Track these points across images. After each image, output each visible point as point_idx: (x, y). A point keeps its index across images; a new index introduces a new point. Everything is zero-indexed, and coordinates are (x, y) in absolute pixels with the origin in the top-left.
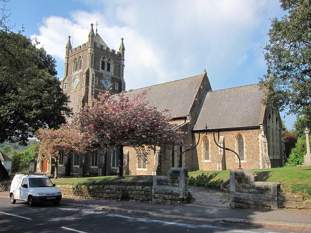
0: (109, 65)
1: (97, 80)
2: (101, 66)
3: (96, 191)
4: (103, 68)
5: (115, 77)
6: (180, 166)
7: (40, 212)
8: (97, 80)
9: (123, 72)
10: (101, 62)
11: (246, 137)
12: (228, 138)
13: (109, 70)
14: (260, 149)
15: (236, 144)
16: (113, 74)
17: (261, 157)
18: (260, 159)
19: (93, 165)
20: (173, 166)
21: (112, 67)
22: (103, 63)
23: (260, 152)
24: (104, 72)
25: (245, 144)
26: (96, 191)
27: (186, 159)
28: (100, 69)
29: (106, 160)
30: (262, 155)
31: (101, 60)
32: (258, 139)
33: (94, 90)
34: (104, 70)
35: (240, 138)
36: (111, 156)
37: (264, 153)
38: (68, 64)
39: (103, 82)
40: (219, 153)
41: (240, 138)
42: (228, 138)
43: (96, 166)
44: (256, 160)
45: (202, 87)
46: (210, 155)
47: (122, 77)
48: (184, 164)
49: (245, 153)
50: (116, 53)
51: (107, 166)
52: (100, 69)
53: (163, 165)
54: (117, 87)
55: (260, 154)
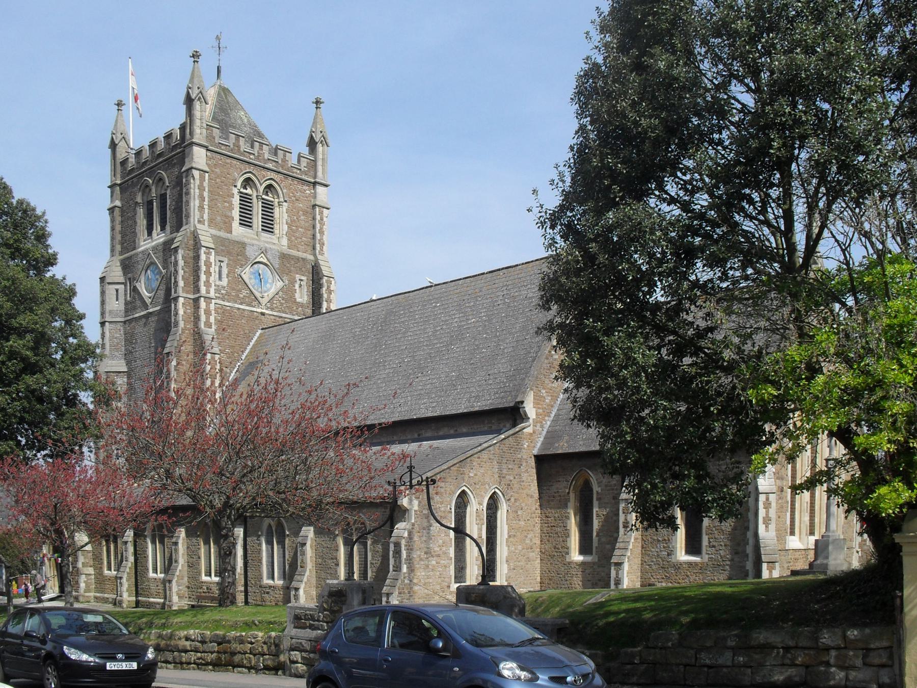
0: (268, 208)
1: (225, 271)
2: (236, 213)
4: (246, 221)
5: (294, 252)
7: (385, 558)
8: (225, 271)
10: (236, 200)
13: (268, 226)
16: (285, 241)
21: (281, 214)
22: (245, 200)
27: (510, 552)
28: (236, 224)
31: (235, 191)
33: (212, 306)
38: (431, 286)
39: (247, 274)
45: (737, 440)
50: (293, 160)
52: (236, 224)
53: (420, 573)
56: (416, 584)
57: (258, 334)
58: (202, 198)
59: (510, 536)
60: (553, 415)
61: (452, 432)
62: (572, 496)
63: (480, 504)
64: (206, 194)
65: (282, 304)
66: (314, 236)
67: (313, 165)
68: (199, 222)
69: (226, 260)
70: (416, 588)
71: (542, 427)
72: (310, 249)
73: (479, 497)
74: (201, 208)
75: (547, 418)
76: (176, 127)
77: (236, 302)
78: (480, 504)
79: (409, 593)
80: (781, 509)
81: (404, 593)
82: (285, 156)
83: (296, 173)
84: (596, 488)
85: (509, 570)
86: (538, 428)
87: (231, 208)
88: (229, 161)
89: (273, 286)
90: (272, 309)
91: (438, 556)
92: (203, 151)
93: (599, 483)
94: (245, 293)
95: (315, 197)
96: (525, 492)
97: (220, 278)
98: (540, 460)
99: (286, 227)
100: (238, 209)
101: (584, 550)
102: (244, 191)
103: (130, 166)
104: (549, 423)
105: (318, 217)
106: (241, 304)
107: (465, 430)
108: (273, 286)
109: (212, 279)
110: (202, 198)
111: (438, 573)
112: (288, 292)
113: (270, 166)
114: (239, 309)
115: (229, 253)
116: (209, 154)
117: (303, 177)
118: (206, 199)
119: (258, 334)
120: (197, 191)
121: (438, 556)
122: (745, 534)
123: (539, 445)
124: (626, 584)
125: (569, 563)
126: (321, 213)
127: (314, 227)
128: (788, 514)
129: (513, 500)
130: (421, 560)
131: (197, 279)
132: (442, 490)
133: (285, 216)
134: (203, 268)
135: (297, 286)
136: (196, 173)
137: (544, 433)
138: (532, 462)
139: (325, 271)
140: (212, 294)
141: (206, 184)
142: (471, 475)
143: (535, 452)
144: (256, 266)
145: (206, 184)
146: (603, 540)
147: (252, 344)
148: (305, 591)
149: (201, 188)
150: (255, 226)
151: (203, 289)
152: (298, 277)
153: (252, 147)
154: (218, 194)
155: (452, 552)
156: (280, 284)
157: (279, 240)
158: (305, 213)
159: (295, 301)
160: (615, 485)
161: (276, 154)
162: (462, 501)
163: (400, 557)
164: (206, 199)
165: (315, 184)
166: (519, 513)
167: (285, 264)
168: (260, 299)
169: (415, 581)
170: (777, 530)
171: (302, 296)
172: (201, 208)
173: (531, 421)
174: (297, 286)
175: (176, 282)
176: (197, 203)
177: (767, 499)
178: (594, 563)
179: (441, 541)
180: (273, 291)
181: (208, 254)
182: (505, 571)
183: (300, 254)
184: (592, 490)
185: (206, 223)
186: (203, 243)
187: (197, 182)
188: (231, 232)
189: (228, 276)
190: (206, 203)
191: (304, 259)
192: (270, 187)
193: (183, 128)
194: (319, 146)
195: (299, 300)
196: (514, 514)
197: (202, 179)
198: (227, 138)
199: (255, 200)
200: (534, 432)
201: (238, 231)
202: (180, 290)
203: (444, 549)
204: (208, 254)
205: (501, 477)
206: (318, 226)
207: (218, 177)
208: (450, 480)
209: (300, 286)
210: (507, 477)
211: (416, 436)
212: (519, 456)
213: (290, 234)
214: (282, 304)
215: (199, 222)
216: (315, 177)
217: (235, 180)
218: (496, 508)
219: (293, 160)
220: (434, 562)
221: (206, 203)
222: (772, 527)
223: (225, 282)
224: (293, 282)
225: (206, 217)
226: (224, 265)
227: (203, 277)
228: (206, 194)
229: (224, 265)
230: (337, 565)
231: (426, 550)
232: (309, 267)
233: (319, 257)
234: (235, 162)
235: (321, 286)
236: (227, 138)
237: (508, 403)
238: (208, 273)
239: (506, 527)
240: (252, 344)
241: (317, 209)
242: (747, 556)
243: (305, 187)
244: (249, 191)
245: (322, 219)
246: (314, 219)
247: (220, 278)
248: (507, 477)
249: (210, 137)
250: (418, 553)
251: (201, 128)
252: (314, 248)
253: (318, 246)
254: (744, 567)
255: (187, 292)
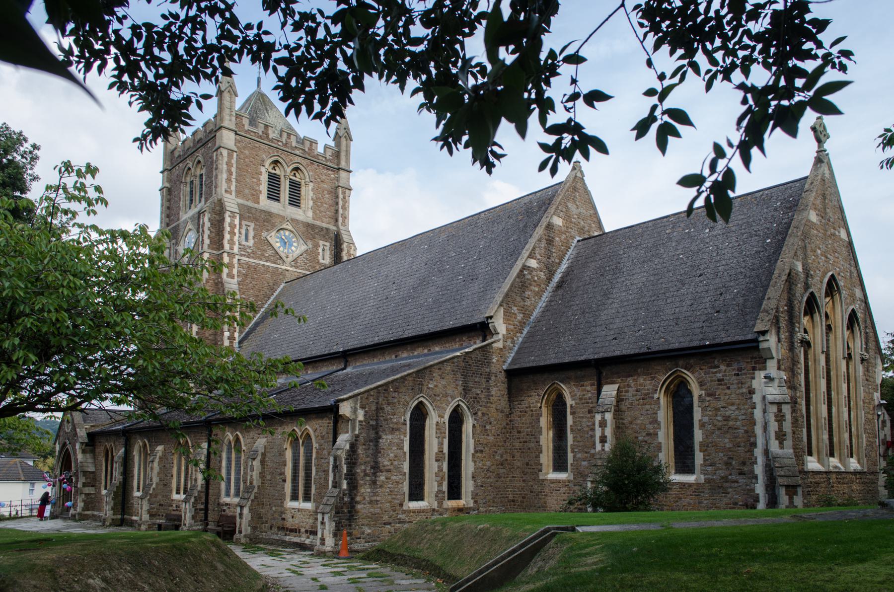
0: (295, 187)
1: (251, 234)
2: (264, 188)
3: (225, 572)
4: (274, 196)
5: (318, 223)
6: (454, 491)
8: (251, 234)
9: (345, 208)
10: (264, 178)
11: (701, 384)
12: (632, 390)
13: (295, 200)
14: (758, 430)
15: (664, 415)
16: (310, 214)
17: (760, 460)
18: (759, 469)
19: (295, 497)
20: (417, 493)
21: (307, 193)
22: (274, 180)
23: (760, 441)
24: (281, 208)
25: (697, 415)
26: (225, 572)
29: (207, 481)
30: (766, 452)
31: (263, 170)
32: (752, 392)
34: (278, 200)
35: (679, 395)
36: (220, 462)
37: (774, 446)
39: (274, 238)
40: (599, 447)
41: (679, 395)
42: (632, 390)
43: (307, 498)
44: (742, 473)
46: (570, 456)
47: (345, 223)
48: (467, 485)
49: (697, 447)
50: (320, 149)
51: (212, 499)
53: (365, 490)
54: (327, 253)
55: (758, 452)
56: (358, 503)
57: (282, 286)
58: (230, 173)
59: (476, 452)
60: (525, 332)
61: (426, 351)
62: (544, 410)
63: (441, 416)
64: (234, 170)
65: (306, 264)
66: (337, 211)
67: (337, 155)
68: (226, 191)
69: (252, 225)
70: (359, 507)
71: (513, 342)
72: (332, 221)
73: (440, 409)
74: (229, 180)
75: (518, 335)
76: (212, 117)
77: (261, 260)
78: (441, 416)
79: (349, 512)
80: (795, 422)
81: (343, 512)
82: (311, 145)
83: (323, 160)
84: (569, 401)
85: (476, 486)
86: (509, 343)
87: (259, 183)
88: (258, 145)
89: (297, 248)
90: (296, 267)
91: (389, 471)
92: (232, 135)
93: (573, 396)
94: (270, 252)
95: (338, 180)
96: (494, 406)
97: (247, 239)
98: (511, 374)
99: (311, 203)
100: (266, 185)
101: (560, 465)
102: (273, 171)
103: (176, 154)
104: (521, 339)
105: (341, 196)
106: (267, 261)
107: (437, 349)
108: (297, 248)
109: (236, 238)
110: (230, 173)
111: (388, 490)
112: (312, 255)
113: (297, 152)
114: (264, 266)
115: (255, 220)
116: (238, 137)
117: (328, 164)
118: (234, 174)
119: (282, 286)
120: (225, 166)
121: (389, 471)
122: (751, 452)
123: (509, 360)
124: (561, 224)
125: (543, 480)
126: (344, 193)
127: (337, 204)
128: (805, 430)
129: (480, 414)
130: (366, 475)
131: (222, 237)
132: (395, 400)
133: (311, 194)
134: (228, 229)
135: (320, 250)
136: (225, 152)
137: (516, 349)
138: (502, 377)
139: (345, 237)
140: (236, 249)
141: (234, 161)
142: (431, 386)
143: (505, 367)
144: (282, 232)
145: (234, 161)
146: (579, 456)
147: (275, 294)
148: (250, 510)
149: (229, 164)
150: (282, 200)
151: (227, 247)
152: (321, 243)
153: (281, 136)
154: (245, 173)
155: (406, 467)
156: (304, 248)
157: (305, 213)
158: (330, 192)
159: (318, 262)
160: (590, 398)
161: (303, 144)
162: (419, 415)
163: (340, 471)
164: (234, 174)
165: (339, 169)
166: (488, 427)
167: (310, 231)
168: (285, 259)
169: (358, 499)
170: (795, 448)
171: (326, 258)
172: (229, 180)
173: (500, 336)
174: (320, 250)
175: (203, 240)
176: (225, 176)
177: (780, 410)
178: (569, 481)
179: (392, 455)
180: (298, 252)
181: (233, 217)
182: (472, 488)
183: (324, 225)
184: (565, 404)
185: (233, 193)
186: (228, 208)
187: (226, 159)
188: (258, 203)
189: (254, 238)
190: (234, 176)
191: (327, 229)
192: (297, 169)
193: (215, 117)
194: (343, 140)
195: (321, 261)
196: (481, 429)
197: (230, 156)
198: (256, 127)
199: (282, 179)
200: (504, 347)
201: (265, 203)
202: (206, 247)
203: (396, 463)
204: (233, 217)
205: (466, 390)
206: (341, 203)
207: (247, 157)
208: (404, 389)
209: (323, 250)
210: (474, 390)
211: (394, 357)
212: (487, 370)
213: (316, 208)
214: (306, 264)
215: (226, 191)
216: (338, 165)
217: (263, 161)
218: (461, 422)
219: (320, 149)
220: (383, 478)
221: (234, 176)
222: (789, 443)
223: (251, 242)
224: (316, 246)
225: (233, 188)
226: (251, 229)
227: (227, 236)
228: (234, 170)
229: (251, 229)
230: (285, 481)
231: (372, 464)
232: (332, 235)
233: (341, 228)
234: (263, 146)
235: (341, 250)
236: (256, 127)
237: (478, 318)
238: (232, 233)
239: (472, 442)
240: (275, 294)
241: (340, 190)
242: (756, 477)
243: (330, 172)
244: (278, 172)
245: (344, 198)
246: (337, 197)
247: (247, 239)
248: (474, 390)
249: (239, 124)
250: (363, 467)
251: (231, 115)
252: (337, 220)
253: (340, 219)
254: (754, 490)
255: (213, 249)
